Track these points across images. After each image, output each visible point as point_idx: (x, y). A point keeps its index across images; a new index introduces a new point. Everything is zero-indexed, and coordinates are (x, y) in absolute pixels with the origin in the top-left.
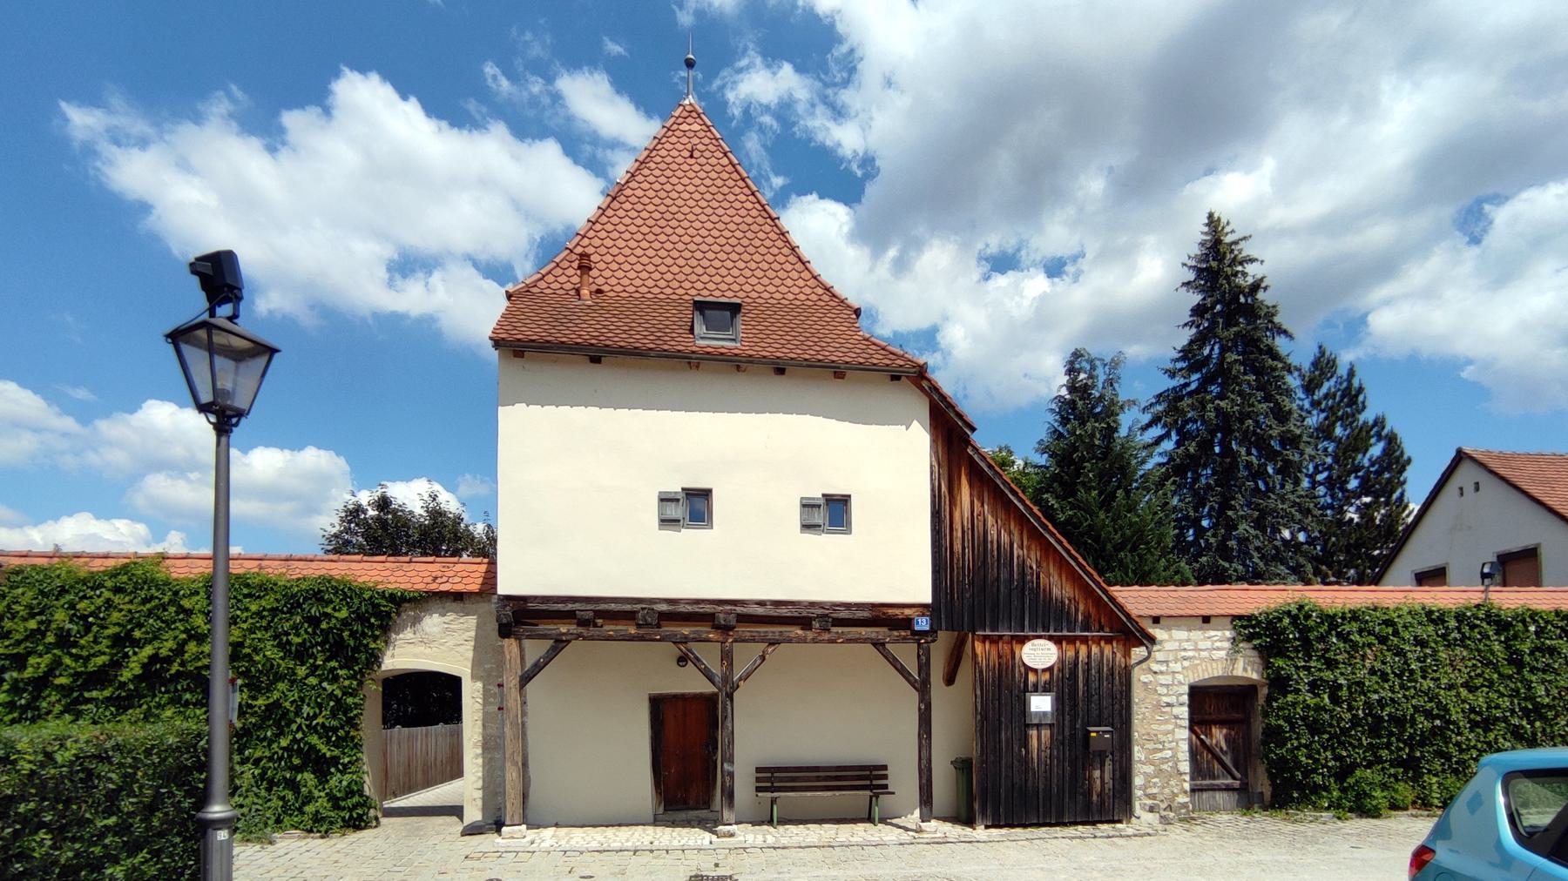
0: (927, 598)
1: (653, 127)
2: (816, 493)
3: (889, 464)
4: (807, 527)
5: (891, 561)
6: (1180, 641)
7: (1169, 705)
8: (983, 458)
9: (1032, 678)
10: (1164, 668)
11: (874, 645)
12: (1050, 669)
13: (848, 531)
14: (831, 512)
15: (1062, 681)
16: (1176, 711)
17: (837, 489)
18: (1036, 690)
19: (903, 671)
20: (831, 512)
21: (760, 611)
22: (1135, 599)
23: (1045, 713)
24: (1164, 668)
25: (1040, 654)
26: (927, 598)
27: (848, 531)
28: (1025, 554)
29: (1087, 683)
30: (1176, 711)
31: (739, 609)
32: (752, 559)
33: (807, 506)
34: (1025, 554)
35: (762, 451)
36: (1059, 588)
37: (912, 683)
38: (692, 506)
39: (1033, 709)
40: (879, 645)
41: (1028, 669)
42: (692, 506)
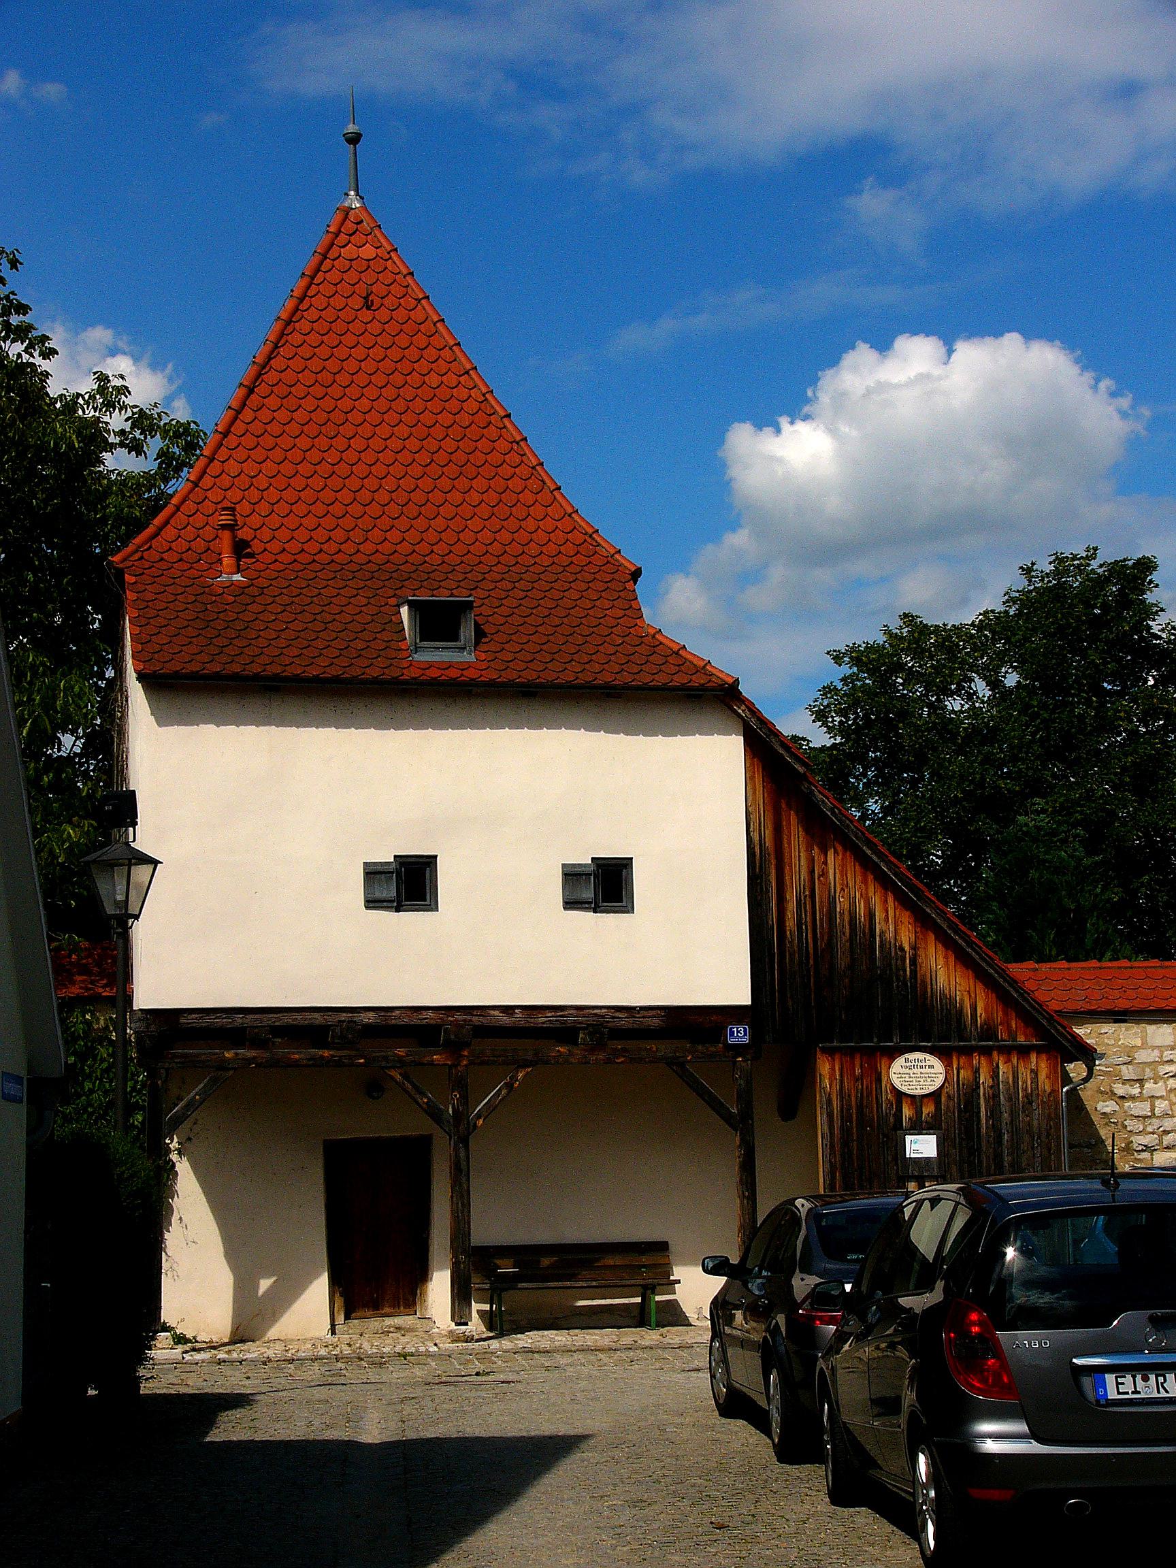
0: (739, 993)
1: (746, 1040)
2: (583, 858)
3: (685, 805)
4: (570, 904)
5: (690, 949)
6: (1161, 1049)
7: (1147, 1148)
8: (798, 759)
9: (907, 1112)
10: (1135, 1091)
11: (669, 1064)
12: (935, 1096)
13: (629, 908)
14: (603, 885)
15: (951, 1114)
16: (133, 579)
17: (612, 850)
18: (918, 1127)
19: (716, 1106)
20: (603, 885)
21: (506, 1020)
22: (1051, 982)
23: (928, 1160)
24: (1135, 1091)
25: (917, 1073)
26: (739, 993)
27: (629, 908)
28: (894, 926)
29: (994, 1111)
30: (133, 579)
31: (476, 1020)
32: (500, 951)
33: (373, 873)
34: (894, 926)
35: (508, 793)
36: (944, 975)
37: (728, 1118)
38: (407, 883)
39: (932, 1139)
40: (676, 1064)
41: (899, 1095)
42: (407, 883)
